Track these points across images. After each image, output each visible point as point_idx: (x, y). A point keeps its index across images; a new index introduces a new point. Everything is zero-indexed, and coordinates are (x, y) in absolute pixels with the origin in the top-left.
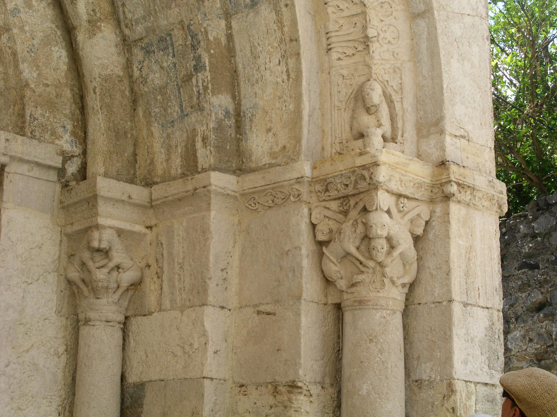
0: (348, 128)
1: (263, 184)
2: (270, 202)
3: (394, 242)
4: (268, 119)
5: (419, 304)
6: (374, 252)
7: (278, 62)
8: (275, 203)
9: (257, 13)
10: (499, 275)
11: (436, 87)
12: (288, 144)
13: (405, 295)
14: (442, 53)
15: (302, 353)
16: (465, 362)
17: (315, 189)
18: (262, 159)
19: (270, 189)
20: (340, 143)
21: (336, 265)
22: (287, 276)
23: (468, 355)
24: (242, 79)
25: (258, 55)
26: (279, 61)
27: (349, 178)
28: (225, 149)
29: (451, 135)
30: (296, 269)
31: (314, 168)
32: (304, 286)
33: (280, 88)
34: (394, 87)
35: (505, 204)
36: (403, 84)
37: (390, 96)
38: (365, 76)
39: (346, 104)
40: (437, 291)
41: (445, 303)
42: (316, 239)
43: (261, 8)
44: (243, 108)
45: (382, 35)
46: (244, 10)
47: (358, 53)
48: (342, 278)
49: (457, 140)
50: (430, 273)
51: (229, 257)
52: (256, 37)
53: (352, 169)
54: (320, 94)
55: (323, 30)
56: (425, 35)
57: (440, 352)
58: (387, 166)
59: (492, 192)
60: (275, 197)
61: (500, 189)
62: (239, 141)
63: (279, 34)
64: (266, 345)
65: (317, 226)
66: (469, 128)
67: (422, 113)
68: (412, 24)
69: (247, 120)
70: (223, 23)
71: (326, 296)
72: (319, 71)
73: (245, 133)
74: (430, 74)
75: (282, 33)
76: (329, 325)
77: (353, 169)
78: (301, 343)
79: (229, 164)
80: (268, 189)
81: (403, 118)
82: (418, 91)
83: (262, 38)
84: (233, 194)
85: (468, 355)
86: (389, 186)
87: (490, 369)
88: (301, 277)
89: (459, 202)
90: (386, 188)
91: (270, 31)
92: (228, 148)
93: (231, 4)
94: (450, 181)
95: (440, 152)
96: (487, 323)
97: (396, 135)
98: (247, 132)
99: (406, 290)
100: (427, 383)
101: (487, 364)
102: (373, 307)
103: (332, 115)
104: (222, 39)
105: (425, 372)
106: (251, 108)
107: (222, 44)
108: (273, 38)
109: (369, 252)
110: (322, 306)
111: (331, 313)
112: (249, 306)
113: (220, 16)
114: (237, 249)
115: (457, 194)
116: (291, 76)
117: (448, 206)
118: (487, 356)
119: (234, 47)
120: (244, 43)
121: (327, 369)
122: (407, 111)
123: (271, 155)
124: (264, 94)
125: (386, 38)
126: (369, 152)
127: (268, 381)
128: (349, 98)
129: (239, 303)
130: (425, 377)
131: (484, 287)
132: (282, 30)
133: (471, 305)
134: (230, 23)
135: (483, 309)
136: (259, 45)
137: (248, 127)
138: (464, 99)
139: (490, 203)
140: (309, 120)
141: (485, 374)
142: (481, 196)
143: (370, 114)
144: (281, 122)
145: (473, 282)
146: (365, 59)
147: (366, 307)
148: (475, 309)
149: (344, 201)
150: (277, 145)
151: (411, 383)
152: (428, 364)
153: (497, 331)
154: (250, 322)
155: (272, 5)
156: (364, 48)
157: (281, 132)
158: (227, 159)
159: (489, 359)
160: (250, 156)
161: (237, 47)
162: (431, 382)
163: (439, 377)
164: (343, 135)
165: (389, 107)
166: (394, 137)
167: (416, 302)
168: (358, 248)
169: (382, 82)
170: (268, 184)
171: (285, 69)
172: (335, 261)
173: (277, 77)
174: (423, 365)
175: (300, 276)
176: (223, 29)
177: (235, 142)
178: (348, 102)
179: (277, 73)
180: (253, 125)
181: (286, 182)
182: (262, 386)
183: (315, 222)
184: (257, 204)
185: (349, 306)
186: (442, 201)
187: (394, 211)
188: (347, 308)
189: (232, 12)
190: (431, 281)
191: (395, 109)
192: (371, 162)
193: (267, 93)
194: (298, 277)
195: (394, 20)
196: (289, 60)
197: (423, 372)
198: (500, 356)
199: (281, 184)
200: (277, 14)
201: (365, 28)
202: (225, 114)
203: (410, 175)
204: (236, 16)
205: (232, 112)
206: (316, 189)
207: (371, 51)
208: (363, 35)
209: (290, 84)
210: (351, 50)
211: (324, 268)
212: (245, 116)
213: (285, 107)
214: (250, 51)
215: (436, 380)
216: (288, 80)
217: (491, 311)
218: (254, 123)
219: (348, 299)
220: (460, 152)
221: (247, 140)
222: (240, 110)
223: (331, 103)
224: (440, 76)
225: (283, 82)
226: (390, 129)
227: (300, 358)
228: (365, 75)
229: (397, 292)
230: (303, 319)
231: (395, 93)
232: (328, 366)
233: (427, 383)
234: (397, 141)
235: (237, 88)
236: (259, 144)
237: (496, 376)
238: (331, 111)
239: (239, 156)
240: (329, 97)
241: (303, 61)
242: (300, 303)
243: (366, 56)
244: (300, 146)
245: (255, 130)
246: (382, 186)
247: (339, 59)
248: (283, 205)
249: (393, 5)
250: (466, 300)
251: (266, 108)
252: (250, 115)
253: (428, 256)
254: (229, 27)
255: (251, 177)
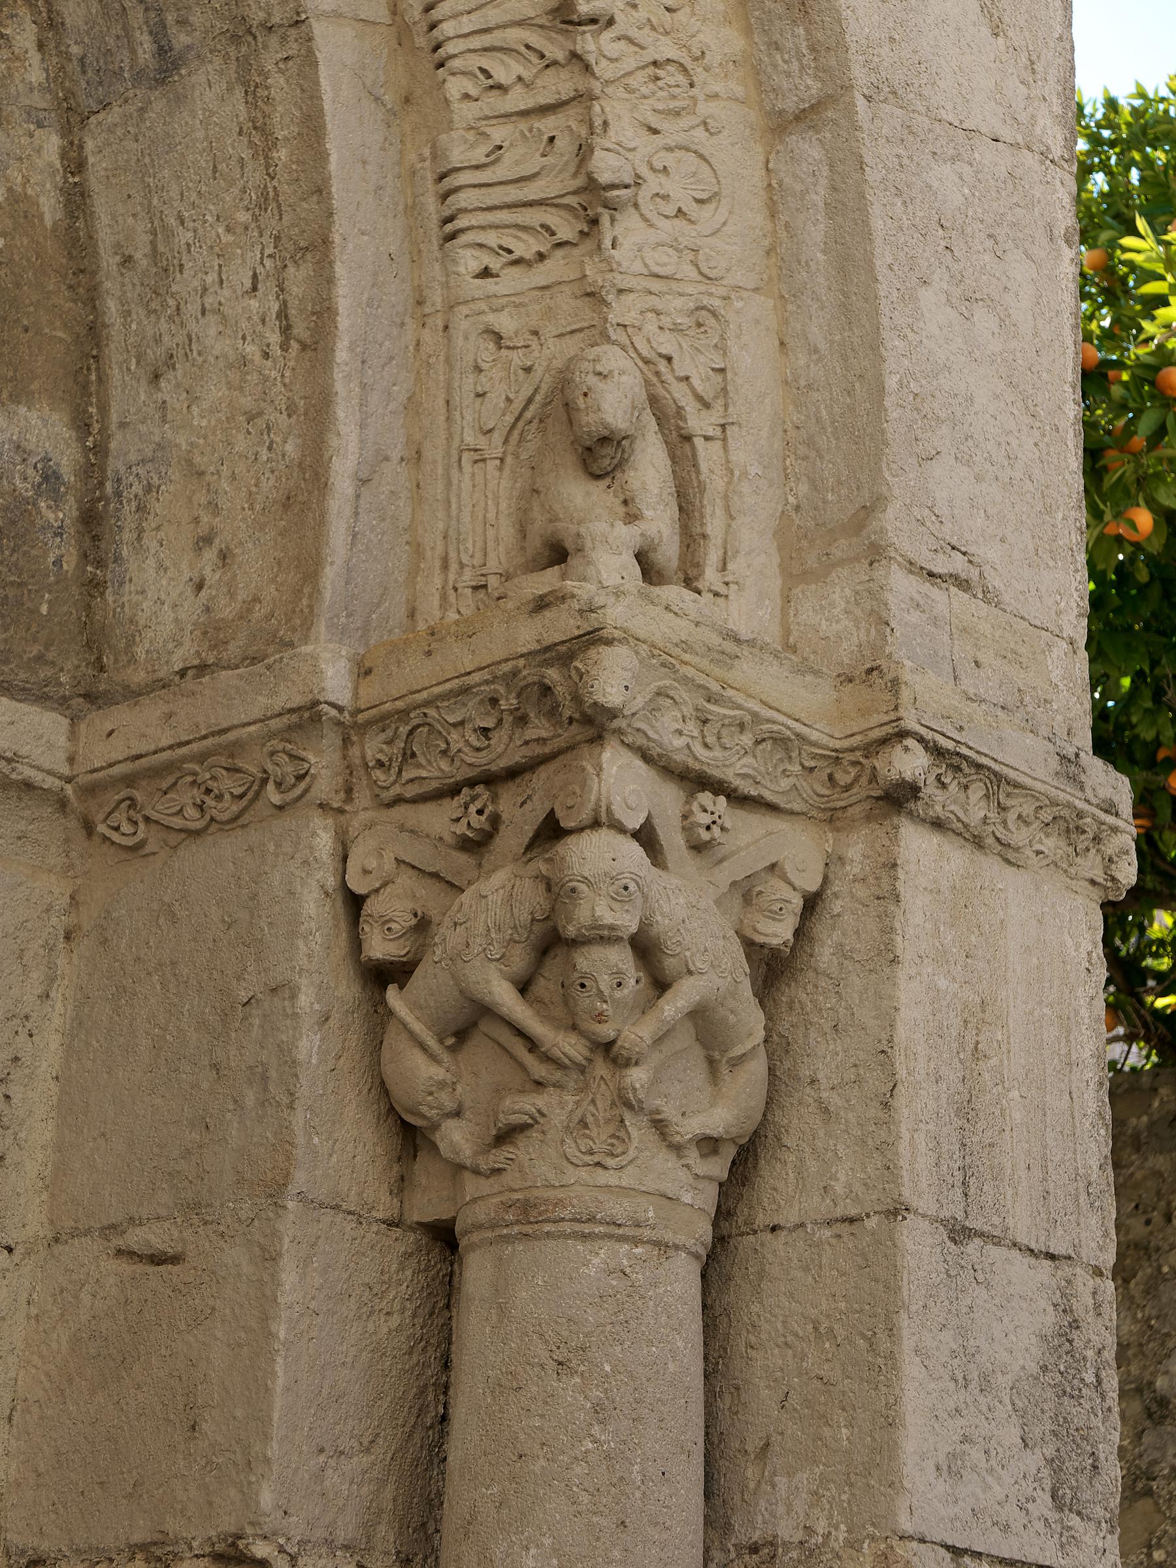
0: (507, 531)
1: (164, 742)
2: (191, 812)
3: (670, 964)
4: (203, 501)
5: (774, 1229)
6: (584, 1001)
7: (248, 284)
8: (207, 817)
9: (180, 100)
10: (1103, 1132)
11: (857, 385)
12: (272, 588)
13: (713, 1191)
14: (883, 258)
15: (276, 1416)
16: (952, 1469)
17: (363, 757)
18: (170, 653)
19: (193, 758)
20: (476, 588)
21: (433, 1058)
22: (236, 1101)
23: (965, 1439)
24: (114, 353)
25: (176, 262)
26: (255, 276)
27: (494, 701)
28: (32, 612)
29: (912, 567)
30: (273, 1074)
31: (363, 671)
32: (300, 1140)
33: (253, 378)
34: (695, 381)
35: (1127, 853)
36: (729, 375)
37: (680, 412)
38: (581, 335)
39: (506, 441)
40: (842, 1178)
41: (872, 1223)
42: (363, 958)
43: (193, 78)
44: (115, 465)
45: (653, 183)
46: (131, 93)
47: (559, 253)
48: (457, 1114)
49: (936, 593)
50: (819, 1101)
51: (23, 1037)
52: (174, 193)
53: (507, 667)
54: (413, 406)
55: (427, 164)
56: (819, 196)
57: (850, 1425)
58: (644, 649)
59: (1067, 794)
60: (208, 791)
61: (1105, 793)
62: (95, 586)
63: (255, 175)
64: (139, 1387)
65: (368, 901)
66: (989, 553)
67: (804, 488)
68: (772, 156)
69: (128, 508)
70: (52, 143)
71: (401, 1185)
72: (408, 320)
73: (118, 559)
74: (838, 338)
75: (267, 167)
76: (403, 1311)
77: (510, 664)
78: (274, 1374)
79: (45, 673)
80: (184, 759)
81: (726, 498)
82: (791, 408)
83: (194, 196)
84: (50, 782)
85: (965, 1439)
86: (651, 733)
87: (1060, 1508)
88: (291, 1107)
89: (938, 825)
90: (640, 741)
91: (222, 167)
92: (44, 609)
93: (84, 72)
94: (903, 734)
95: (868, 631)
96: (1050, 1319)
97: (697, 565)
98: (125, 553)
99: (718, 1167)
100: (794, 1554)
101: (1048, 1488)
102: (578, 1227)
103: (449, 484)
104: (42, 200)
105: (789, 1508)
106: (143, 461)
107: (41, 217)
108: (235, 191)
109: (567, 1001)
110: (375, 1228)
111: (413, 1261)
112: (88, 1232)
113: (42, 115)
114: (59, 1005)
115: (930, 789)
116: (295, 331)
117: (894, 837)
118: (1050, 1451)
119: (91, 238)
120: (130, 220)
121: (389, 1492)
122: (745, 474)
123: (205, 633)
124: (194, 407)
125: (666, 197)
126: (573, 596)
127: (137, 1538)
128: (518, 419)
129: (52, 1222)
130: (787, 1531)
131: (1037, 1172)
132: (266, 157)
133: (981, 1235)
134: (81, 147)
135: (1033, 1261)
136: (182, 223)
137: (127, 535)
138: (970, 443)
139: (1062, 843)
140: (358, 496)
141: (1039, 1526)
142: (1028, 809)
143: (598, 477)
144: (252, 508)
145: (991, 1145)
146: (583, 270)
147: (548, 1228)
148: (993, 1252)
149: (474, 799)
150: (232, 595)
151: (733, 1555)
152: (802, 1477)
153: (1090, 1353)
154: (85, 1297)
155: (233, 66)
156: (581, 232)
157: (250, 545)
158: (35, 652)
159: (1055, 1464)
160: (131, 642)
161: (105, 237)
162: (811, 1551)
163: (843, 1527)
164: (492, 555)
165: (673, 458)
166: (692, 573)
167: (761, 1219)
168: (523, 987)
169: (647, 362)
170: (185, 738)
171: (276, 307)
172: (431, 1042)
173: (244, 338)
174: (781, 1481)
175: (286, 1100)
176: (50, 165)
177: (75, 590)
178: (516, 433)
179: (244, 324)
180: (150, 523)
181: (252, 728)
182: (111, 1560)
183: (358, 886)
184: (142, 826)
185: (480, 1227)
186: (868, 818)
187: (672, 839)
188: (475, 1237)
189: (87, 103)
190: (821, 1133)
191: (695, 465)
192: (577, 633)
193: (205, 405)
194: (279, 1104)
195: (700, 133)
196: (291, 269)
197: (781, 1510)
198: (1102, 1456)
199: (231, 736)
200: (250, 99)
201: (584, 152)
202: (38, 479)
203: (740, 698)
204: (101, 116)
205: (68, 476)
206: (369, 753)
207: (607, 243)
208: (580, 181)
209: (291, 364)
210: (531, 240)
211: (388, 1070)
212: (118, 494)
213: (270, 448)
214: (148, 250)
215: (832, 1544)
216: (284, 347)
217: (1066, 1270)
218: (150, 517)
219: (482, 1198)
220: (946, 638)
221: (121, 584)
222: (103, 471)
223: (450, 437)
224: (875, 346)
225: (266, 355)
226: (677, 538)
227: (266, 1437)
228: (580, 330)
229: (684, 1176)
230: (289, 1277)
231: (698, 406)
232: (393, 1479)
233: (794, 1554)
234: (699, 585)
235: (98, 394)
236: (163, 597)
237: (1087, 1539)
238: (447, 469)
239: (89, 645)
240: (442, 418)
241: (340, 269)
242: (279, 1207)
243: (587, 259)
244: (317, 591)
245: (154, 545)
246: (619, 732)
247: (486, 273)
248: (240, 822)
249: (699, 75)
250: (960, 1215)
251: (197, 459)
252: (137, 488)
253: (813, 1034)
254: (75, 163)
255: (121, 716)
